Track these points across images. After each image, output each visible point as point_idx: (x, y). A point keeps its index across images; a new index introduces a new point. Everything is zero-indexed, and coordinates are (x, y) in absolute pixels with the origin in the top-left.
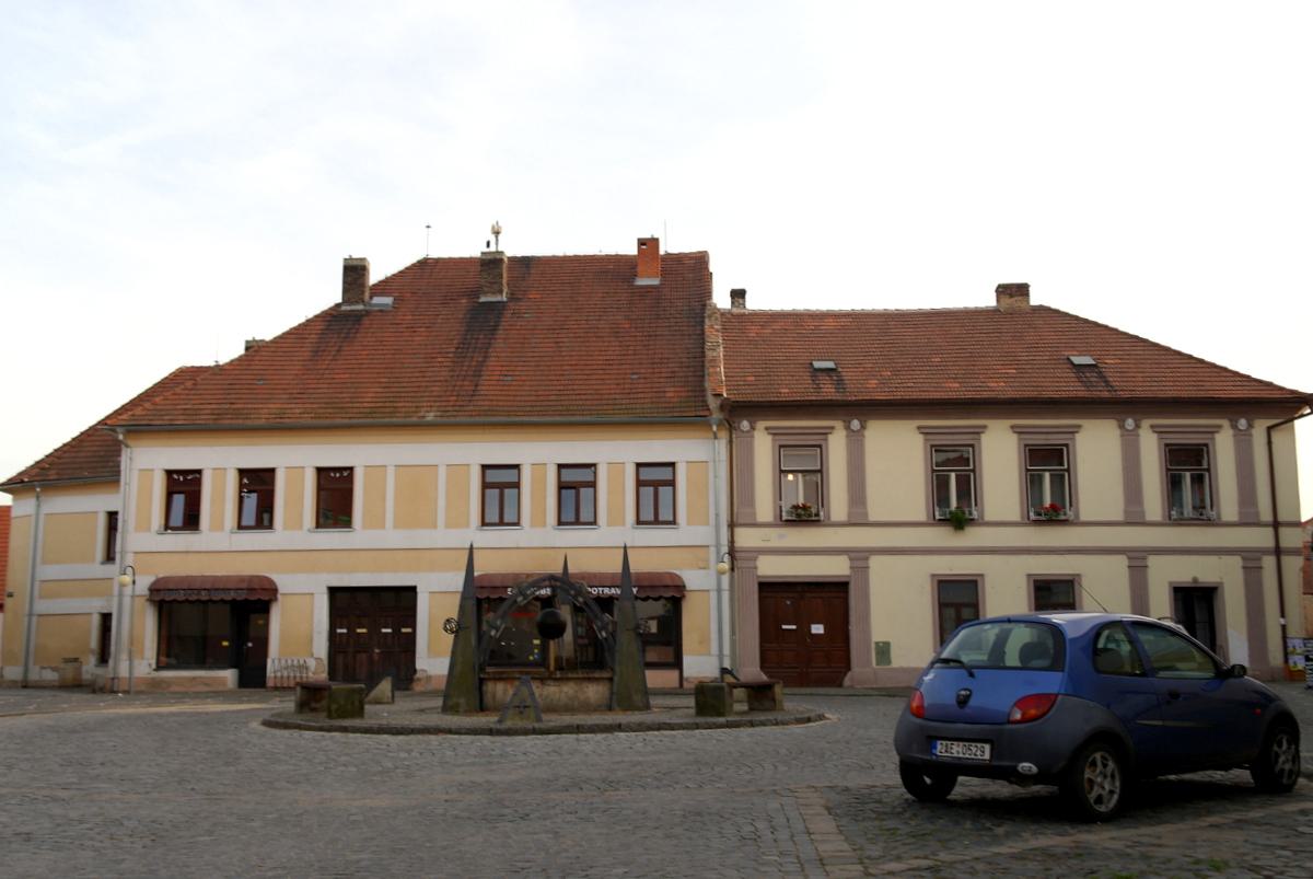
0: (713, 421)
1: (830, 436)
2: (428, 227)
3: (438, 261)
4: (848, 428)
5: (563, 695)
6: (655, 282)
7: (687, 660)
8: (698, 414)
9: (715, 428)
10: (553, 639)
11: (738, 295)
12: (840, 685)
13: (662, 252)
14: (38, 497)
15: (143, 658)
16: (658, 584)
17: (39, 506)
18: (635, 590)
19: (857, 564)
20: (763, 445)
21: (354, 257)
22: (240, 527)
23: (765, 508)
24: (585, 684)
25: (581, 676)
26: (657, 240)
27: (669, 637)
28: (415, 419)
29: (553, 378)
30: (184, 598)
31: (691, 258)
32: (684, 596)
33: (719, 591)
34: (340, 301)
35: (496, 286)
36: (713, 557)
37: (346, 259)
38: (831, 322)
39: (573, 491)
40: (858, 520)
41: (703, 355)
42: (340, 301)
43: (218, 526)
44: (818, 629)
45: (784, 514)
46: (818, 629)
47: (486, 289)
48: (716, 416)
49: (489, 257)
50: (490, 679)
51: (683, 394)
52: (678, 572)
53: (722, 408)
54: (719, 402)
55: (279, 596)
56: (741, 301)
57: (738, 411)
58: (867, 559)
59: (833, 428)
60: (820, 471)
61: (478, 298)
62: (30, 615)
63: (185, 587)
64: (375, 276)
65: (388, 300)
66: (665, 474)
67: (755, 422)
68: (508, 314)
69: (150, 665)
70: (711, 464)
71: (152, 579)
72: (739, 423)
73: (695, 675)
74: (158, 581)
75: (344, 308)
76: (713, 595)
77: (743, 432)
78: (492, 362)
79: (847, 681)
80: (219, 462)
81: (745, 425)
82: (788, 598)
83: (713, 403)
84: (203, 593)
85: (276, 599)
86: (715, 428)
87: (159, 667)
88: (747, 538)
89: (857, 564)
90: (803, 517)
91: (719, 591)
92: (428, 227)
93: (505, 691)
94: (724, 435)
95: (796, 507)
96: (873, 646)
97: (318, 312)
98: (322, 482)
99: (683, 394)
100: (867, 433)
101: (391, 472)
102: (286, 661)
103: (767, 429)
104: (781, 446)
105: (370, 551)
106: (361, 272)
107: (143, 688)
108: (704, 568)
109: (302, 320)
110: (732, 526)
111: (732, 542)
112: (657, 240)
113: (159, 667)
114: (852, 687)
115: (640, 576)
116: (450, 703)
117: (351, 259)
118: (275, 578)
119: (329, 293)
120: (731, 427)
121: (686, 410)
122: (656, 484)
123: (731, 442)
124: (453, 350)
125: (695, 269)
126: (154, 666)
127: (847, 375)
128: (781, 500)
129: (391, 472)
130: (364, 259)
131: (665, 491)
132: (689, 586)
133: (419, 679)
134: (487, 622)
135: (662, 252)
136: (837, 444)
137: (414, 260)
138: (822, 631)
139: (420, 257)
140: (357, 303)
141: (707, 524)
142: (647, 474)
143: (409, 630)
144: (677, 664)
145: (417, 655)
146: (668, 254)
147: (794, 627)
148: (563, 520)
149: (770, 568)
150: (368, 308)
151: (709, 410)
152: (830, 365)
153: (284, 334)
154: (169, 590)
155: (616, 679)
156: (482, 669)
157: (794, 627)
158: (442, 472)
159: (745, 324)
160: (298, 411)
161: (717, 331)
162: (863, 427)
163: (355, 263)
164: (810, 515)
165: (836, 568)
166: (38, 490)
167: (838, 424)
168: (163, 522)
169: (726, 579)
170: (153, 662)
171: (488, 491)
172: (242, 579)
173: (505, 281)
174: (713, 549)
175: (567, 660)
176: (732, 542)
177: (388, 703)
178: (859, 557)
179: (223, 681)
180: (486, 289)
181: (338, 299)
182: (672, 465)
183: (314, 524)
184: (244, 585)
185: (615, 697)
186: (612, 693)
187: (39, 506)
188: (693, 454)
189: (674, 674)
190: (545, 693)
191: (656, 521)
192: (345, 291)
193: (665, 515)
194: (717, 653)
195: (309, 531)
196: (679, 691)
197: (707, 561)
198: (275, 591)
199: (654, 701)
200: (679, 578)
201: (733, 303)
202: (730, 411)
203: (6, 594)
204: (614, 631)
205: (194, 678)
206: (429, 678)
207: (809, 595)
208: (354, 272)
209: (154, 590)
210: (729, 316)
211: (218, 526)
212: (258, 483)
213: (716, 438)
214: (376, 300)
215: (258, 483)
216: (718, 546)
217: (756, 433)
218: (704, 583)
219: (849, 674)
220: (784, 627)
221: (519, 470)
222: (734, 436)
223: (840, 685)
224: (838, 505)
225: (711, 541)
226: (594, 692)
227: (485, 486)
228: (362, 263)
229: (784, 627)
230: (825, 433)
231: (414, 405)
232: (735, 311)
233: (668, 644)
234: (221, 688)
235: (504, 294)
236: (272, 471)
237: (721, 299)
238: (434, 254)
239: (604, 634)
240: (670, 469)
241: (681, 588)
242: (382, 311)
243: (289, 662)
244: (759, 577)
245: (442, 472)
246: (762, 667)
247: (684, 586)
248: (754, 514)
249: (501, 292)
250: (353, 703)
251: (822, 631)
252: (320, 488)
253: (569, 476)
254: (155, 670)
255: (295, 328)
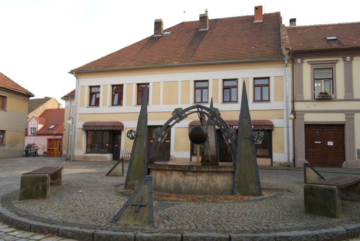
0: (285, 59)
1: (336, 64)
2: (184, 12)
3: (187, 23)
4: (345, 60)
5: (199, 182)
6: (261, 21)
7: (274, 155)
8: (279, 57)
9: (286, 62)
10: (199, 144)
11: (293, 21)
12: (341, 167)
13: (263, 13)
14: (70, 101)
15: (81, 149)
16: (262, 124)
17: (71, 103)
18: (253, 127)
19: (348, 117)
20: (306, 69)
21: (158, 19)
22: (113, 105)
23: (307, 94)
24: (215, 175)
25: (211, 170)
26: (262, 6)
27: (266, 146)
28: (170, 64)
29: (222, 50)
30: (92, 129)
31: (273, 14)
32: (273, 129)
33: (288, 127)
34: (153, 34)
35: (204, 26)
36: (285, 114)
37: (155, 20)
38: (331, 28)
39: (229, 90)
40: (349, 98)
41: (280, 39)
42: (153, 34)
43: (105, 105)
44: (330, 143)
45: (316, 96)
46: (330, 143)
47: (201, 27)
48: (287, 58)
49: (202, 16)
50: (154, 169)
51: (272, 51)
52: (270, 120)
53: (289, 54)
54: (288, 52)
55: (124, 129)
56: (294, 23)
57: (296, 55)
58: (353, 114)
59: (338, 60)
60: (332, 79)
61: (199, 30)
62: (69, 136)
63: (93, 125)
64: (165, 27)
65: (169, 33)
66: (265, 82)
67: (303, 59)
68: (208, 33)
69: (84, 152)
70: (284, 77)
71: (85, 122)
72: (297, 60)
73: (277, 161)
74: (86, 123)
75: (155, 36)
76: (285, 129)
77: (298, 64)
78: (200, 47)
79: (344, 165)
80: (106, 82)
81: (299, 61)
82: (317, 131)
83: (285, 52)
84: (99, 127)
85: (123, 130)
86: (286, 62)
87: (87, 152)
88: (299, 106)
89: (348, 117)
90: (324, 97)
91: (288, 127)
92: (184, 12)
93: (161, 178)
94: (290, 65)
95: (322, 93)
96: (356, 151)
97: (146, 37)
98: (139, 89)
99: (272, 51)
100: (353, 62)
101: (162, 84)
102: (128, 151)
103: (308, 62)
104: (314, 69)
105: (158, 113)
106: (160, 24)
107: (81, 159)
108: (282, 118)
109: (141, 40)
110: (293, 101)
111: (293, 108)
112: (262, 6)
113: (87, 152)
114: (346, 168)
115: (254, 121)
116: (129, 183)
117: (157, 20)
118: (123, 122)
119: (150, 32)
120: (293, 61)
121: (274, 57)
122: (262, 86)
123: (293, 68)
124: (188, 44)
125: (277, 16)
126: (85, 152)
127: (342, 41)
128: (314, 91)
129: (162, 84)
130: (161, 20)
131: (265, 89)
132: (275, 125)
133: (171, 159)
134: (156, 133)
135: (263, 13)
136: (340, 68)
137: (180, 23)
138: (332, 144)
139: (182, 21)
140: (159, 34)
141: (283, 101)
142: (258, 82)
143: (169, 141)
144: (270, 156)
145: (171, 151)
146: (265, 14)
147: (320, 142)
148: (225, 100)
149: (310, 118)
150: (162, 35)
151: (284, 55)
152: (335, 38)
153: (134, 44)
154: (88, 126)
155: (237, 172)
156: (151, 162)
157: (320, 142)
158: (180, 84)
159: (295, 30)
160: (131, 64)
161: (285, 31)
162: (352, 60)
163: (158, 21)
164: (328, 97)
165: (339, 118)
166: (70, 98)
167: (340, 59)
168: (88, 104)
169: (291, 122)
170: (85, 150)
171: (197, 90)
172: (111, 123)
173: (208, 24)
174: (285, 111)
175: (212, 156)
176: (293, 108)
177: (120, 176)
178: (350, 114)
179: (106, 158)
180: (201, 27)
181: (153, 34)
182: (268, 78)
183: (136, 104)
184: (111, 125)
185: (236, 185)
186: (234, 182)
187: (71, 103)
188: (278, 74)
189: (269, 160)
190: (186, 181)
191: (262, 100)
192: (155, 30)
193: (265, 98)
194: (287, 152)
195: (134, 106)
196: (271, 167)
197: (283, 115)
198: (123, 127)
199: (264, 193)
200: (271, 122)
201: (290, 24)
202: (293, 55)
203: (64, 129)
204: (237, 139)
205: (97, 157)
206: (175, 159)
207: (326, 129)
208: (158, 24)
209: (84, 126)
210: (289, 28)
211: (105, 105)
212: (118, 90)
213: (287, 66)
214: (165, 33)
215: (118, 90)
216: (287, 110)
217: (304, 64)
218: (282, 127)
219: (345, 162)
220: (316, 142)
221: (208, 82)
222: (294, 65)
223: (341, 167)
224: (340, 93)
225: (284, 108)
226: (221, 181)
227: (196, 88)
228: (160, 21)
229: (316, 142)
230: (334, 63)
231: (171, 60)
232: (292, 26)
233: (267, 148)
234: (105, 160)
235: (207, 28)
236: (122, 85)
237: (286, 23)
238: (186, 21)
239: (230, 141)
240: (268, 80)
241: (272, 126)
242: (167, 36)
243: (129, 152)
244: (304, 122)
245: (180, 84)
246: (306, 158)
247: (273, 126)
248: (303, 97)
249: (206, 27)
250: (37, 188)
251: (332, 144)
252: (138, 91)
253: (227, 84)
254: (85, 153)
255: (138, 42)
